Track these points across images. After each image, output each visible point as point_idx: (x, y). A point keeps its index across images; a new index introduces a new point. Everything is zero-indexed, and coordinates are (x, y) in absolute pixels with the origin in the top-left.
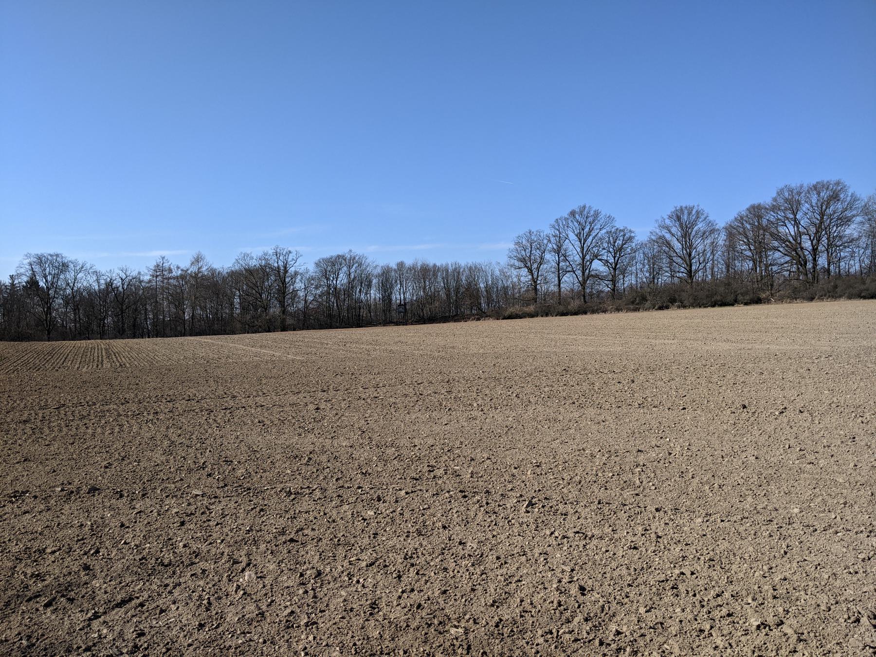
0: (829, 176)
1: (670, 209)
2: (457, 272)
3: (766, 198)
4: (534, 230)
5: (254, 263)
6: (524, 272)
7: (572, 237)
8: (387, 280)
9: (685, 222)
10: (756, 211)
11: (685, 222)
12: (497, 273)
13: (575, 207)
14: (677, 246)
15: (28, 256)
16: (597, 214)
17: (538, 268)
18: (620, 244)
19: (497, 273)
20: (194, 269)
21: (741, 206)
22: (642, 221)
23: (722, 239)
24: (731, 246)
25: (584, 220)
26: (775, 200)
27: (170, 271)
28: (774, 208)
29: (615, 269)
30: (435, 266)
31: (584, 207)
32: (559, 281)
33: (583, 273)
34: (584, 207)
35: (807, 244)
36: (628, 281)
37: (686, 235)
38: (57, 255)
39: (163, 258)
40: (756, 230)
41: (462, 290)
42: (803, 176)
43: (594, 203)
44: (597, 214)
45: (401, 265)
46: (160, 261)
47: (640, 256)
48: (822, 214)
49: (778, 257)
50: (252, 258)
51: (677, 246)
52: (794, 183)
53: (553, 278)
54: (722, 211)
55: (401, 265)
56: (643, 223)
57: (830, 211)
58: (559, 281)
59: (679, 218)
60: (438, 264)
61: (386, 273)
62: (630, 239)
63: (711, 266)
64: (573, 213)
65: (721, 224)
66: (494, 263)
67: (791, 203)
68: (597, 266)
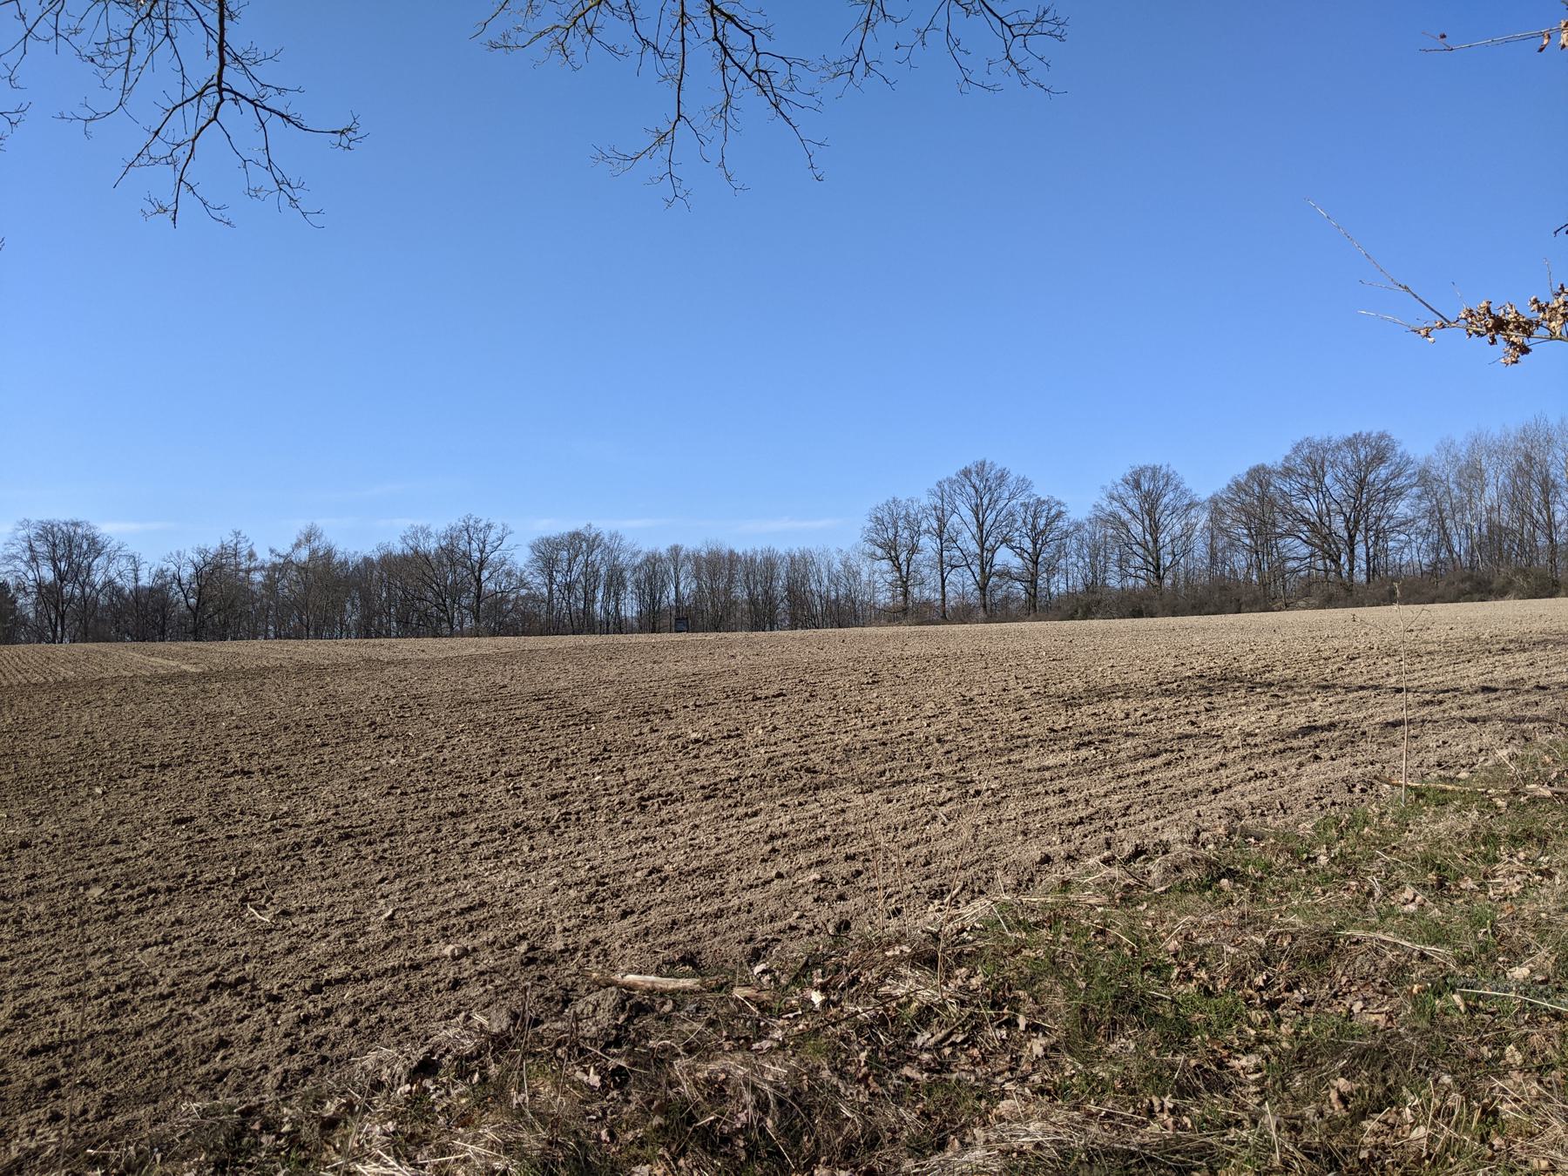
0: (1370, 425)
1: (1123, 470)
2: (770, 564)
3: (1273, 456)
4: (903, 498)
5: (431, 546)
6: (886, 565)
7: (966, 512)
8: (653, 573)
9: (1149, 493)
10: (1259, 475)
11: (1149, 493)
12: (837, 566)
13: (969, 462)
14: (1137, 529)
15: (26, 523)
16: (1002, 477)
17: (909, 561)
18: (1043, 530)
19: (837, 566)
20: (303, 555)
21: (1239, 469)
22: (1080, 489)
23: (1202, 519)
24: (1216, 527)
25: (982, 484)
26: (1287, 458)
27: (251, 555)
28: (1288, 472)
29: (1036, 563)
30: (732, 553)
31: (983, 464)
32: (943, 581)
33: (983, 570)
34: (983, 464)
35: (1338, 524)
36: (1059, 586)
37: (1151, 504)
38: (76, 524)
39: (237, 534)
40: (1258, 505)
41: (761, 606)
42: (1334, 425)
43: (998, 460)
44: (1002, 477)
45: (675, 551)
46: (229, 539)
47: (1072, 544)
48: (1361, 483)
49: (1296, 549)
50: (429, 535)
51: (1137, 529)
52: (1318, 435)
53: (934, 579)
54: (1207, 474)
55: (675, 551)
56: (1081, 492)
57: (1371, 477)
58: (943, 581)
59: (1137, 485)
60: (739, 550)
61: (653, 560)
62: (1059, 515)
63: (1190, 541)
64: (966, 473)
65: (1204, 493)
66: (833, 549)
67: (1313, 464)
68: (1005, 557)
